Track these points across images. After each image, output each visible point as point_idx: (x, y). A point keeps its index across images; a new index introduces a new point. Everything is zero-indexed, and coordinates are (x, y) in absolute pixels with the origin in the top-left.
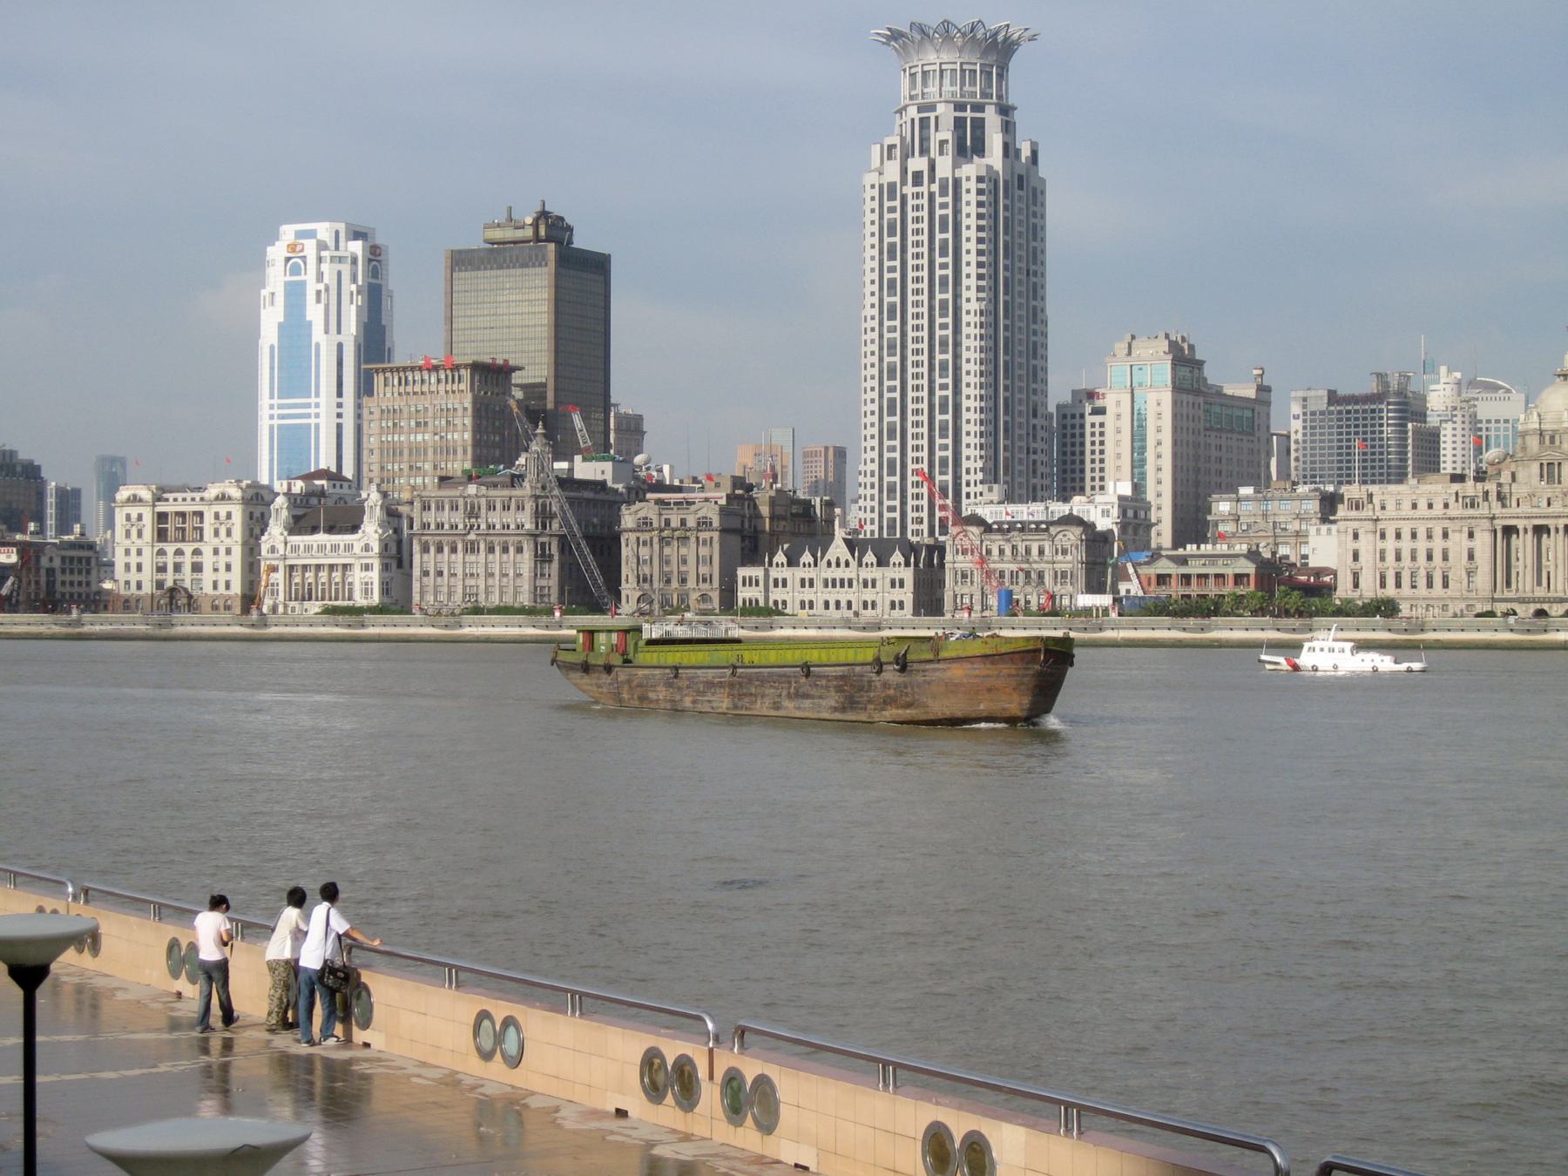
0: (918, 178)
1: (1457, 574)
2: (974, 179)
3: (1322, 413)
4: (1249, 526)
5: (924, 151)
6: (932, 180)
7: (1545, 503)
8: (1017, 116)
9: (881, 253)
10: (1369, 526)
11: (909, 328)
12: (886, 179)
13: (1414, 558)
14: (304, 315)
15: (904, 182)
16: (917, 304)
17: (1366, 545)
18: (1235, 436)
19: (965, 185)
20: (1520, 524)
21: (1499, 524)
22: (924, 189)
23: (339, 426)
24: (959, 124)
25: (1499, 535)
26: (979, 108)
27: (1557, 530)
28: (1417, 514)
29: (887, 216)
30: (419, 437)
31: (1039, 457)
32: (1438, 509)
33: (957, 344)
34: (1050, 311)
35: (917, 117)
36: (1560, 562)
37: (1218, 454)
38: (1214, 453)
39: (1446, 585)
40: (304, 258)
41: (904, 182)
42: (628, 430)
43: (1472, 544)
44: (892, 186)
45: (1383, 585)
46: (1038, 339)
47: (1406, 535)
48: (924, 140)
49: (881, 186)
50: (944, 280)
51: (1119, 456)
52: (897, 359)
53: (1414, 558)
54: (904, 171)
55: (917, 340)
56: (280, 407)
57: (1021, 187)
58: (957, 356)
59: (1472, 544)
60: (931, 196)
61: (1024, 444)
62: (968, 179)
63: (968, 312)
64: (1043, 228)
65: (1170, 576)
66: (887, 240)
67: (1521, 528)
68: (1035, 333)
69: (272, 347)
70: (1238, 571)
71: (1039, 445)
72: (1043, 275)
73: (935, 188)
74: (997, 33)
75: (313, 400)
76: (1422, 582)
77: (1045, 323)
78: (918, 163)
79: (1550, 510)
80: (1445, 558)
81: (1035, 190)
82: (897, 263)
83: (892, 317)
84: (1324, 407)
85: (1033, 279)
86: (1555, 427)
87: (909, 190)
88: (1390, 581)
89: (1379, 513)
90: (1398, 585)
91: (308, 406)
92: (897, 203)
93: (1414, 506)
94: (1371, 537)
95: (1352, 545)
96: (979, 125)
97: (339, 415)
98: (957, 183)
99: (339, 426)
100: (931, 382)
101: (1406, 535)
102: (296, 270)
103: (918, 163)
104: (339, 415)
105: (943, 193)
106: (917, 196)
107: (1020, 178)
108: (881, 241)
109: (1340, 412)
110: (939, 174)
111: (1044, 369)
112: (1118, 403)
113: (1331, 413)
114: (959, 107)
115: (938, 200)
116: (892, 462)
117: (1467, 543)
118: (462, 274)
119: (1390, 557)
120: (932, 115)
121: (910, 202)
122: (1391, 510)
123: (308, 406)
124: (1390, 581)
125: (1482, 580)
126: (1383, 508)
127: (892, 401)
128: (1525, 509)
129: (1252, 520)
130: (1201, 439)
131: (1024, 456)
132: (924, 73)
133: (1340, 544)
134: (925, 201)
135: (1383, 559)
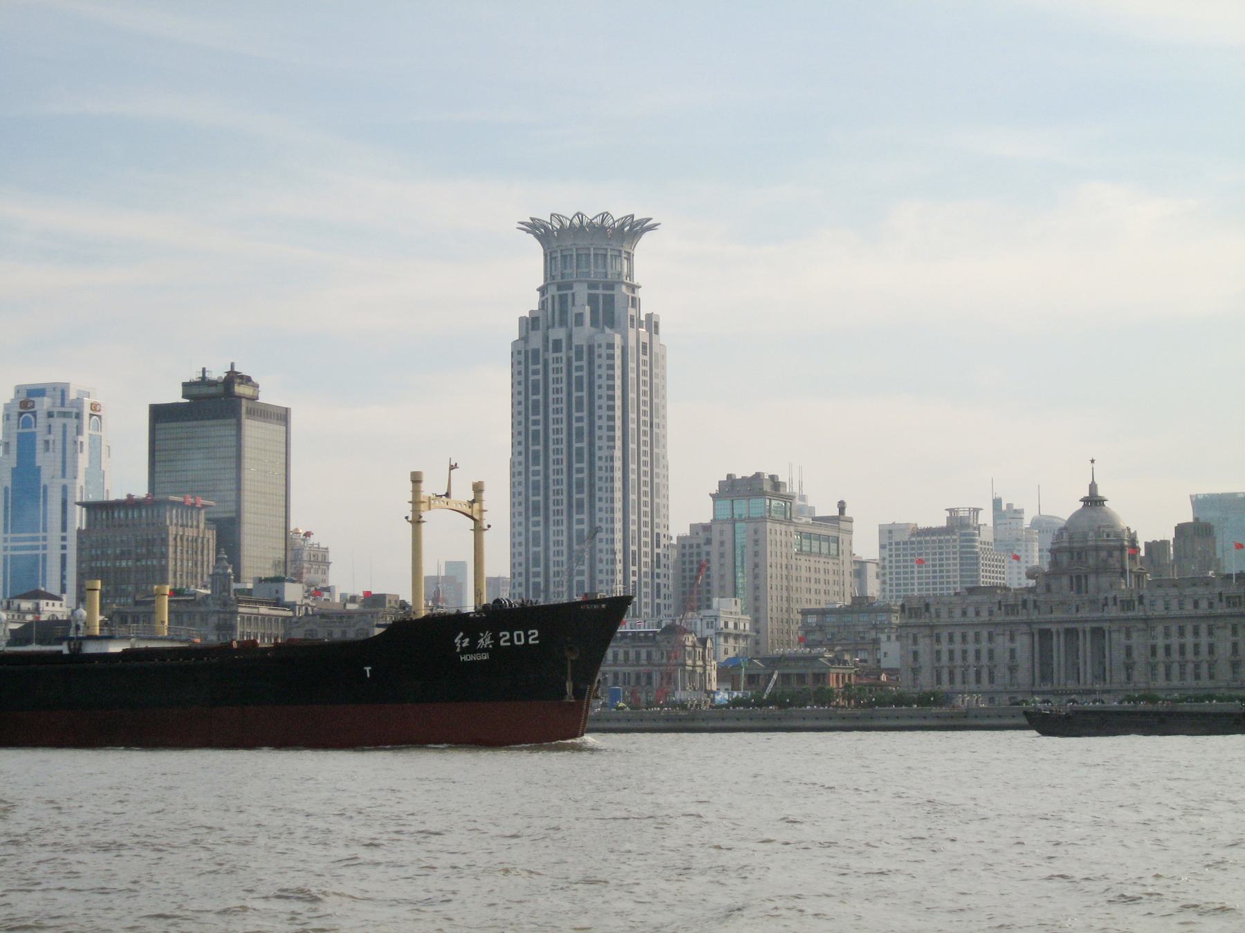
0: (557, 345)
1: (1002, 673)
2: (604, 346)
3: (905, 543)
4: (833, 634)
5: (563, 322)
6: (569, 347)
7: (1074, 610)
9: (526, 408)
10: (927, 631)
11: (551, 472)
13: (1197, 653)
14: (34, 463)
15: (546, 349)
16: (557, 451)
17: (924, 646)
18: (822, 560)
20: (1054, 628)
21: (1036, 627)
22: (563, 354)
23: (64, 557)
24: (592, 300)
25: (1036, 638)
26: (610, 286)
27: (1084, 632)
28: (967, 620)
29: (531, 378)
30: (124, 564)
31: (661, 581)
32: (985, 616)
34: (669, 457)
35: (556, 293)
36: (1089, 660)
37: (808, 575)
38: (804, 574)
39: (992, 680)
40: (34, 414)
41: (546, 349)
42: (316, 562)
43: (1013, 645)
44: (536, 352)
45: (939, 681)
47: (958, 638)
48: (563, 312)
49: (526, 352)
51: (722, 577)
52: (541, 498)
53: (1197, 653)
54: (546, 339)
55: (557, 503)
56: (14, 540)
58: (591, 394)
59: (1210, 640)
63: (600, 458)
65: (759, 675)
66: (532, 398)
67: (1054, 630)
69: (6, 489)
70: (816, 671)
71: (661, 571)
72: (664, 427)
75: (41, 534)
76: (972, 677)
78: (558, 333)
79: (1079, 615)
80: (991, 657)
82: (540, 417)
83: (536, 462)
84: (906, 538)
86: (1080, 545)
87: (551, 355)
88: (945, 677)
89: (935, 621)
90: (952, 681)
91: (36, 539)
92: (540, 367)
93: (964, 613)
94: (927, 641)
95: (912, 648)
97: (64, 547)
98: (591, 349)
99: (64, 557)
101: (958, 638)
102: (26, 424)
104: (64, 547)
106: (557, 360)
108: (527, 398)
109: (920, 542)
110: (575, 342)
112: (722, 532)
113: (912, 543)
114: (593, 286)
115: (575, 364)
116: (536, 454)
117: (1008, 645)
118: (162, 425)
119: (1161, 652)
120: (569, 292)
122: (945, 617)
123: (36, 539)
124: (945, 677)
125: (1023, 676)
126: (938, 616)
127: (536, 534)
128: (1057, 615)
129: (836, 630)
130: (793, 562)
131: (649, 580)
132: (578, 255)
133: (902, 647)
134: (564, 365)
135: (939, 659)
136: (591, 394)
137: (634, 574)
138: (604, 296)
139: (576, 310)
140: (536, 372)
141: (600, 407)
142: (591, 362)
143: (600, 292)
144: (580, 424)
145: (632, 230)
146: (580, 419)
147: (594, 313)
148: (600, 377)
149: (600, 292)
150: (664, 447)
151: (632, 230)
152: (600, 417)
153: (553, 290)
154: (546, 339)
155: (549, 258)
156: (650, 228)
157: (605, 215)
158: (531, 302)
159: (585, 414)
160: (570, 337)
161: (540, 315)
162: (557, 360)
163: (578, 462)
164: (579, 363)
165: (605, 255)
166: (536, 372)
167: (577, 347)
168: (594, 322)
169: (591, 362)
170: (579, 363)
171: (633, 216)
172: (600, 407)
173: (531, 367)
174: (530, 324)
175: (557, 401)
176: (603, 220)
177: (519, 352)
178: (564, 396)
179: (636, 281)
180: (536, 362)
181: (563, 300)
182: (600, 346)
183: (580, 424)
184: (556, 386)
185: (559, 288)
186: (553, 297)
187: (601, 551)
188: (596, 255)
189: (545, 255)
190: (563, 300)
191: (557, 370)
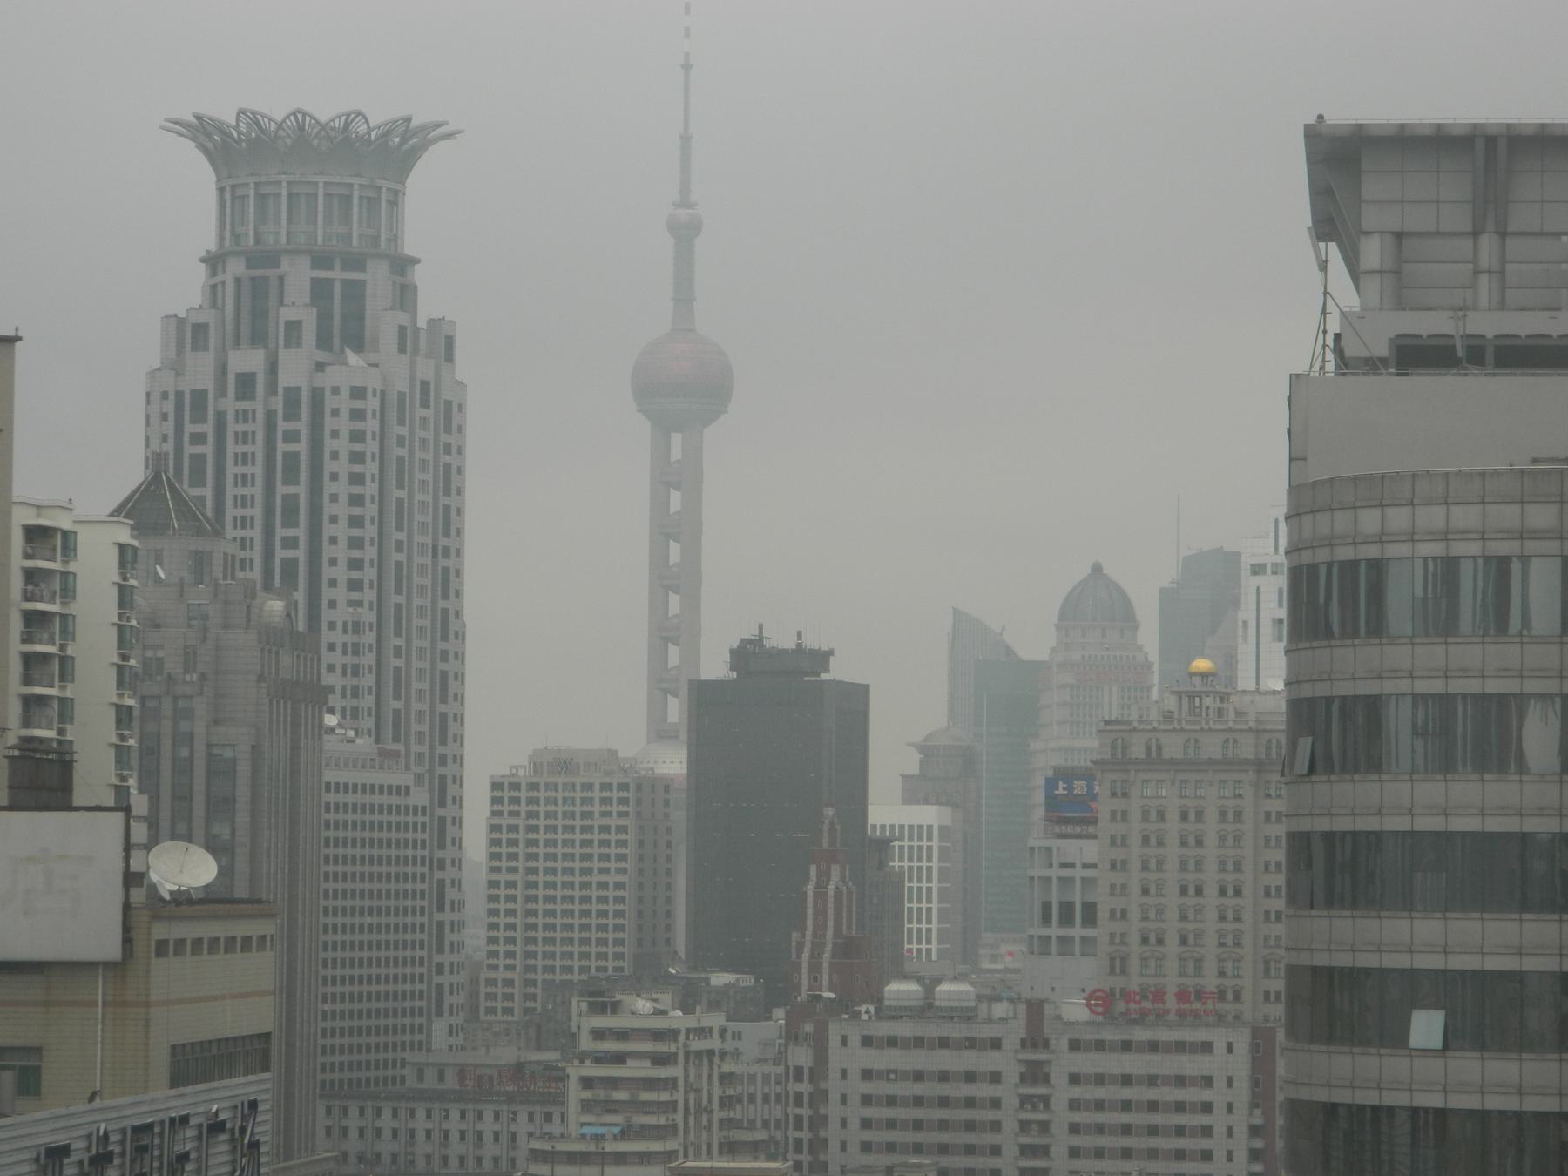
0: (246, 384)
2: (345, 392)
5: (258, 337)
6: (272, 389)
8: (419, 275)
12: (187, 385)
15: (222, 392)
19: (330, 402)
22: (258, 406)
24: (320, 291)
26: (355, 262)
33: (316, 510)
34: (468, 616)
41: (222, 392)
44: (199, 397)
46: (449, 770)
48: (260, 315)
49: (179, 395)
50: (290, 518)
54: (222, 370)
57: (425, 404)
58: (316, 490)
60: (270, 417)
61: (429, 540)
62: (336, 391)
64: (460, 677)
68: (447, 449)
72: (459, 553)
73: (278, 403)
74: (387, 134)
77: (461, 636)
78: (249, 360)
81: (449, 404)
85: (442, 562)
87: (230, 405)
92: (208, 428)
96: (355, 292)
98: (317, 397)
100: (270, 426)
103: (249, 360)
105: (292, 411)
107: (425, 385)
110: (285, 379)
111: (459, 718)
115: (282, 426)
121: (232, 427)
131: (428, 560)
132: (290, 195)
134: (259, 428)
136: (316, 490)
137: (398, 654)
138: (345, 282)
139: (287, 314)
140: (199, 439)
141: (334, 519)
142: (316, 426)
143: (337, 274)
144: (290, 553)
145: (389, 153)
146: (290, 543)
147: (324, 318)
148: (334, 477)
149: (337, 274)
150: (459, 492)
151: (389, 153)
152: (334, 498)
153: (236, 267)
154: (222, 370)
155: (230, 198)
156: (449, 136)
157: (352, 116)
158: (187, 290)
159: (301, 532)
160: (273, 368)
161: (207, 317)
162: (244, 416)
163: (286, 482)
164: (291, 426)
165: (349, 198)
166: (199, 439)
167: (287, 390)
168: (324, 341)
169: (316, 426)
170: (291, 426)
171: (408, 120)
172: (333, 541)
173: (189, 428)
174: (189, 334)
175: (244, 459)
176: (347, 125)
177: (165, 395)
178: (258, 491)
179: (409, 251)
180: (199, 417)
181: (258, 288)
182: (336, 391)
183: (290, 553)
184: (241, 491)
185: (253, 260)
186: (238, 281)
187: (334, 498)
188: (328, 196)
189: (221, 190)
190: (258, 288)
191: (245, 438)
